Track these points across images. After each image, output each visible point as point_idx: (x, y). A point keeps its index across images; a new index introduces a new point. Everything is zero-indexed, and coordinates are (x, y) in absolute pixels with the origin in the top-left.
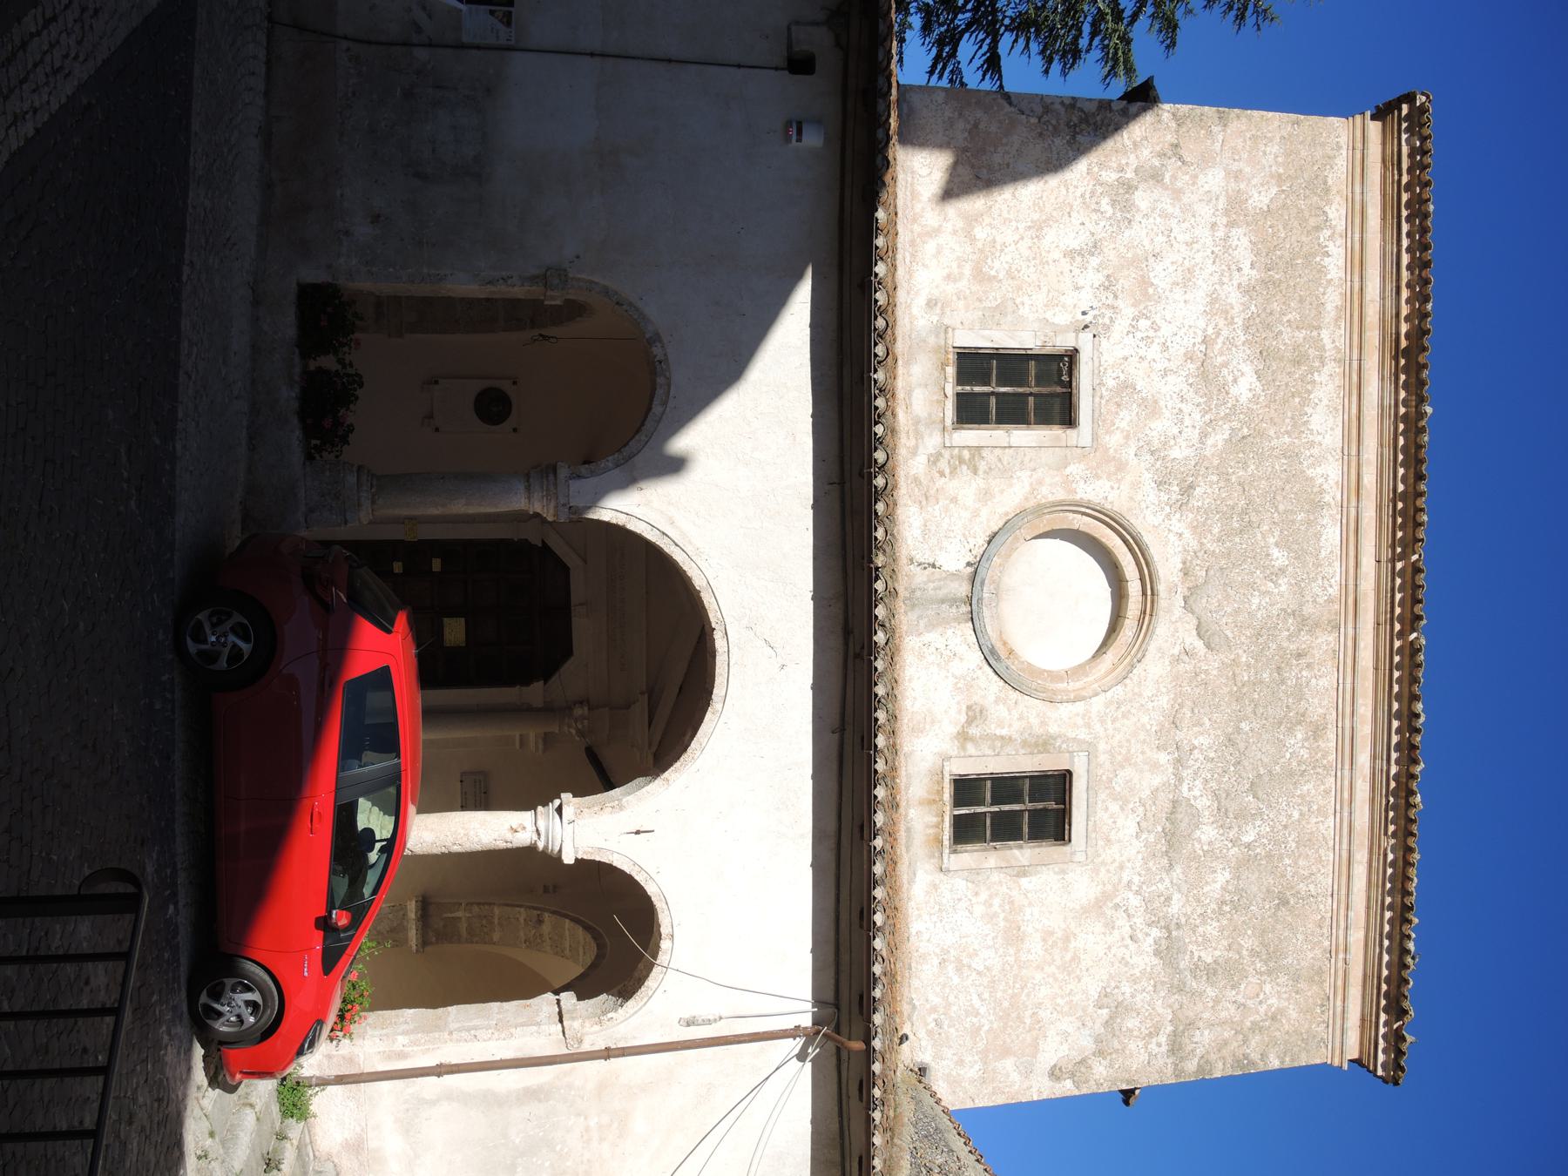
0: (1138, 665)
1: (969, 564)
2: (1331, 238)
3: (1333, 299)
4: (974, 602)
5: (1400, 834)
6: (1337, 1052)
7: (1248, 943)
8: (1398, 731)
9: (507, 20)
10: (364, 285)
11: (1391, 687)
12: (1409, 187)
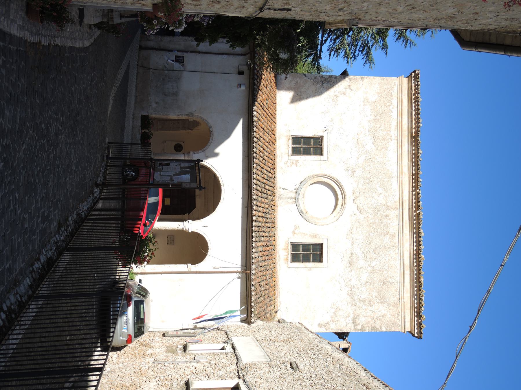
0: (341, 217)
1: (295, 189)
2: (393, 108)
3: (394, 124)
4: (297, 198)
5: (418, 266)
6: (403, 328)
7: (375, 294)
8: (416, 237)
9: (183, 65)
10: (154, 116)
11: (413, 225)
12: (414, 94)
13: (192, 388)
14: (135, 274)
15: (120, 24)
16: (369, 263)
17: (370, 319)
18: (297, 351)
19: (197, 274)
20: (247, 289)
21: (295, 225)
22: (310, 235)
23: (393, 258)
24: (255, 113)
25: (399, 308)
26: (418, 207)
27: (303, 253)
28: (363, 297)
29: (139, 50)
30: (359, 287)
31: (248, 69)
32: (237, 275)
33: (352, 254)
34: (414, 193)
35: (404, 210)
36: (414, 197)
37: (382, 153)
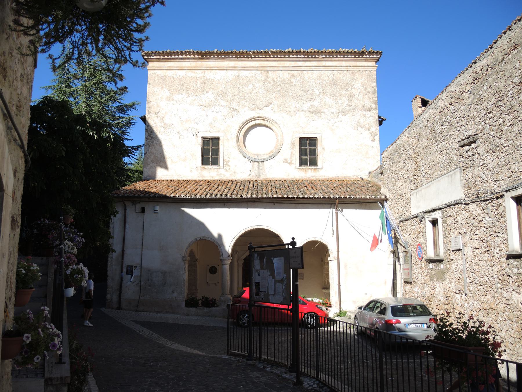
1: (250, 162)
3: (190, 74)
5: (318, 54)
6: (373, 68)
7: (344, 92)
8: (293, 55)
9: (136, 267)
11: (282, 57)
12: (164, 56)
13: (519, 251)
14: (341, 311)
15: (72, 364)
16: (316, 97)
17: (366, 96)
18: (436, 144)
19: (339, 251)
20: (353, 202)
21: (284, 162)
22: (293, 149)
23: (311, 76)
24: (182, 196)
25: (356, 71)
26: (266, 53)
27: (308, 155)
28: (347, 102)
29: (121, 310)
30: (338, 105)
31: (139, 203)
32: (339, 213)
33: (309, 111)
34: (253, 56)
35: (268, 66)
36: (257, 56)
37: (217, 85)
